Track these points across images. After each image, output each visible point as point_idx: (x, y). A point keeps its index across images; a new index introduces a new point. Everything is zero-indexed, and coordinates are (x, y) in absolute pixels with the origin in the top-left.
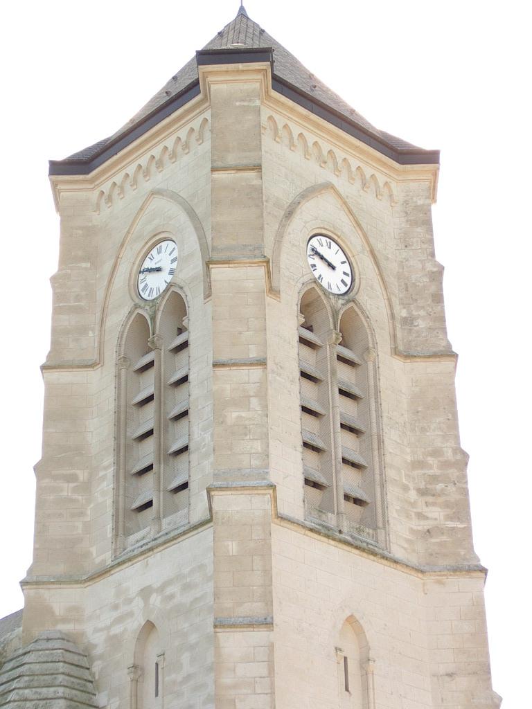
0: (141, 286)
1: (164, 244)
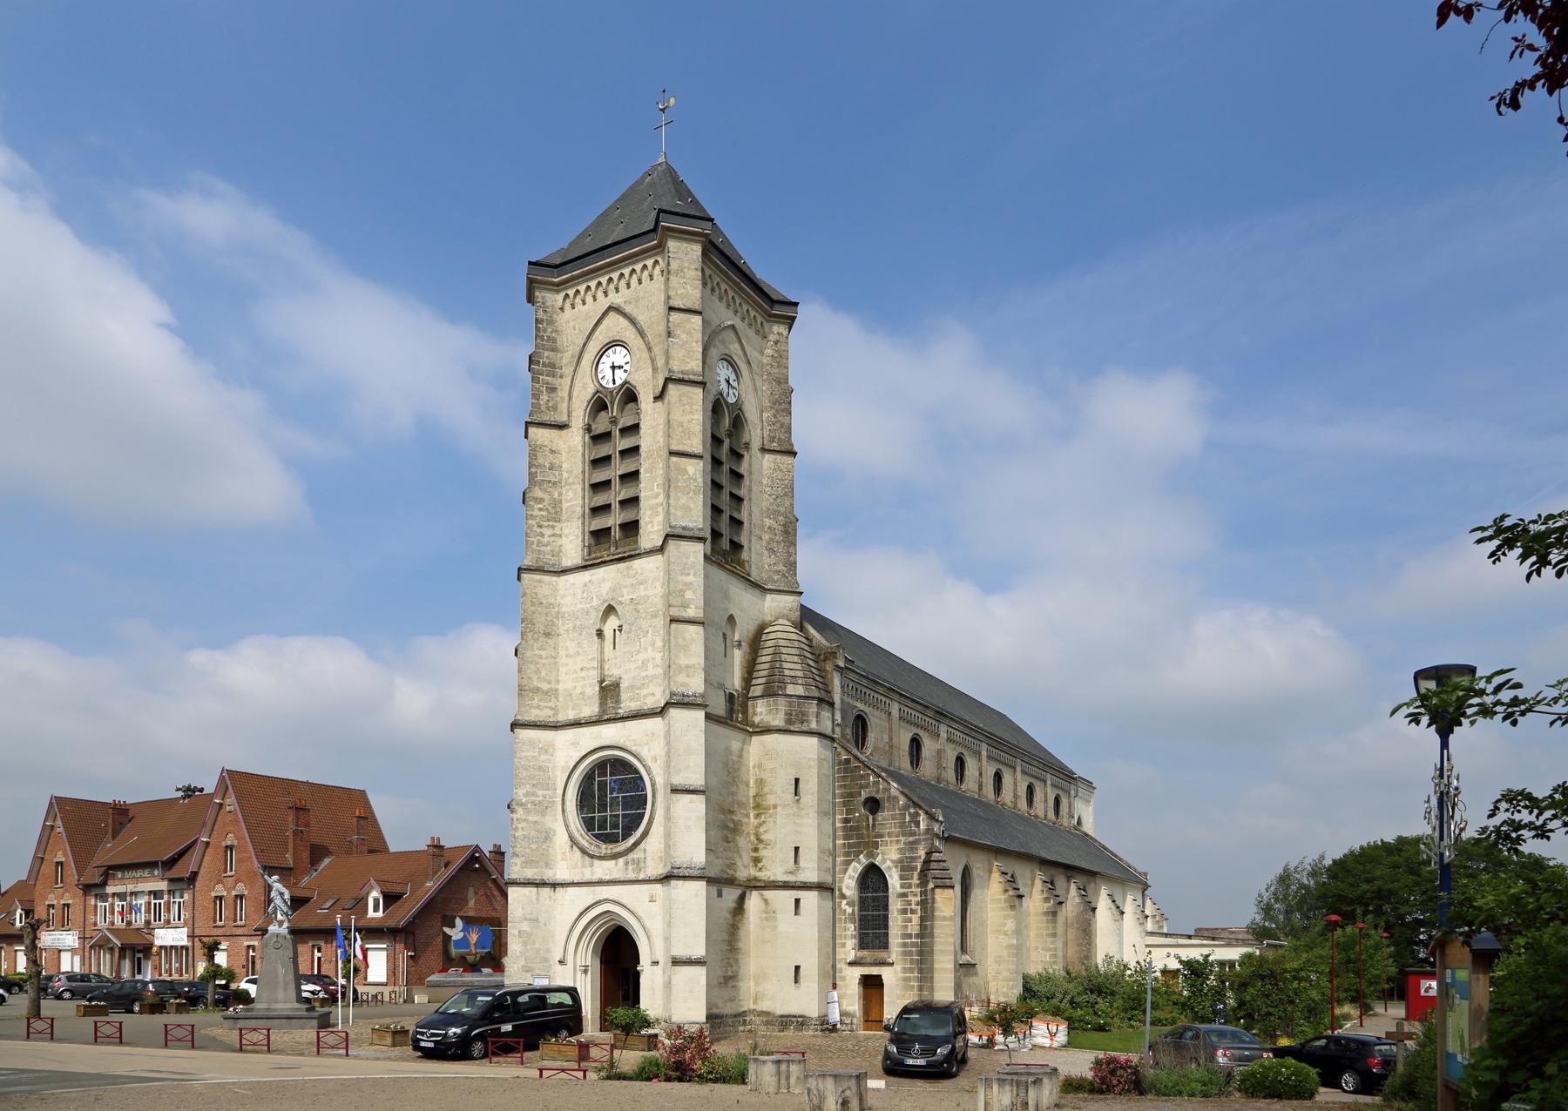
0: (600, 376)
1: (618, 348)
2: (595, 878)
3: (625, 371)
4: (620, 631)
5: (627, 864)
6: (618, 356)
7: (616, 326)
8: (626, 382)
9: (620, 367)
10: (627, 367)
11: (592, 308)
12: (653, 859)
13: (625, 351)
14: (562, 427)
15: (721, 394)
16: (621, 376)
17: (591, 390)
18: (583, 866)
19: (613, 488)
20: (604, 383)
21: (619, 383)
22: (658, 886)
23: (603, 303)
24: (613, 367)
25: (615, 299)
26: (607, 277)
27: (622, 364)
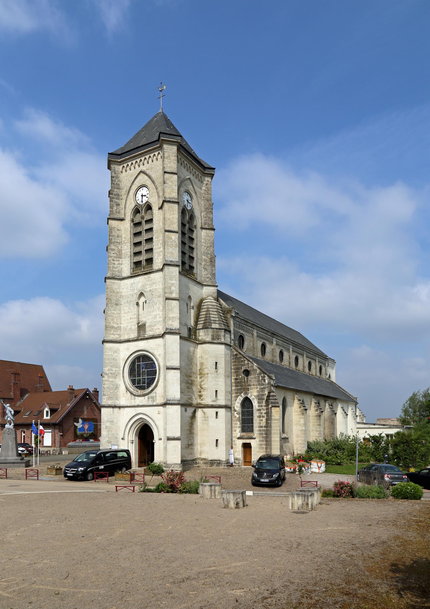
0: (137, 199)
1: (144, 188)
2: (136, 404)
3: (147, 197)
4: (146, 303)
5: (149, 398)
6: (144, 191)
7: (143, 179)
8: (147, 202)
9: (145, 196)
10: (148, 196)
11: (134, 172)
12: (159, 396)
13: (147, 189)
14: (122, 220)
15: (185, 206)
16: (145, 199)
17: (133, 205)
18: (131, 399)
19: (142, 245)
20: (138, 202)
21: (144, 202)
22: (161, 407)
23: (138, 170)
24: (142, 196)
25: (143, 168)
26: (139, 159)
27: (146, 194)
